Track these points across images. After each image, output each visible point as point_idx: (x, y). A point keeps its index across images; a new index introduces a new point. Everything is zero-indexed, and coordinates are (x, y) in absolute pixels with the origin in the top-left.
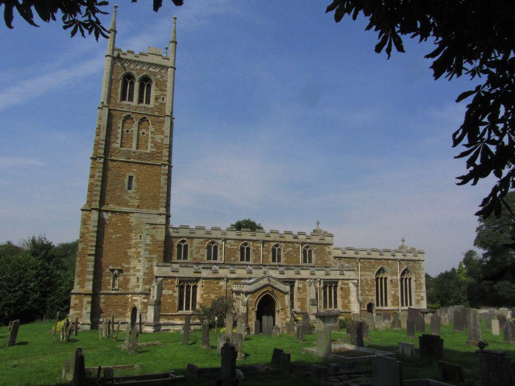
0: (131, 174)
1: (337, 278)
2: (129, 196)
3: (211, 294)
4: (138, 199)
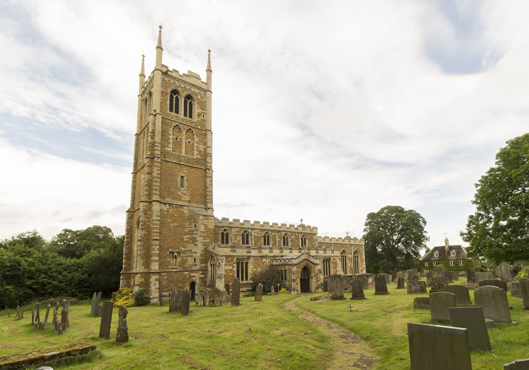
0: (183, 175)
1: (330, 255)
2: (182, 193)
3: (258, 268)
4: (189, 195)
